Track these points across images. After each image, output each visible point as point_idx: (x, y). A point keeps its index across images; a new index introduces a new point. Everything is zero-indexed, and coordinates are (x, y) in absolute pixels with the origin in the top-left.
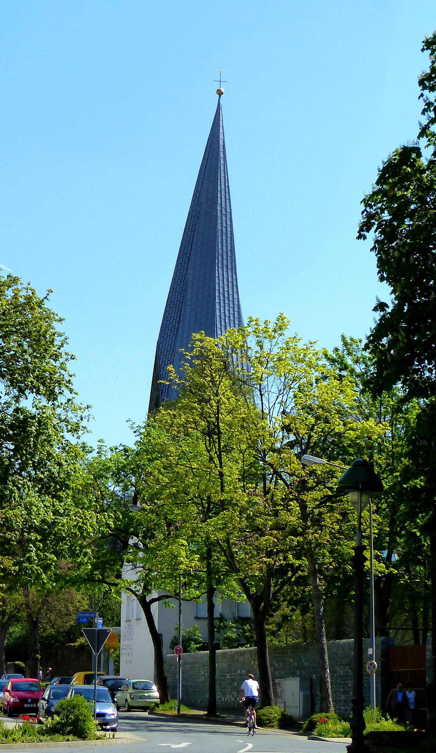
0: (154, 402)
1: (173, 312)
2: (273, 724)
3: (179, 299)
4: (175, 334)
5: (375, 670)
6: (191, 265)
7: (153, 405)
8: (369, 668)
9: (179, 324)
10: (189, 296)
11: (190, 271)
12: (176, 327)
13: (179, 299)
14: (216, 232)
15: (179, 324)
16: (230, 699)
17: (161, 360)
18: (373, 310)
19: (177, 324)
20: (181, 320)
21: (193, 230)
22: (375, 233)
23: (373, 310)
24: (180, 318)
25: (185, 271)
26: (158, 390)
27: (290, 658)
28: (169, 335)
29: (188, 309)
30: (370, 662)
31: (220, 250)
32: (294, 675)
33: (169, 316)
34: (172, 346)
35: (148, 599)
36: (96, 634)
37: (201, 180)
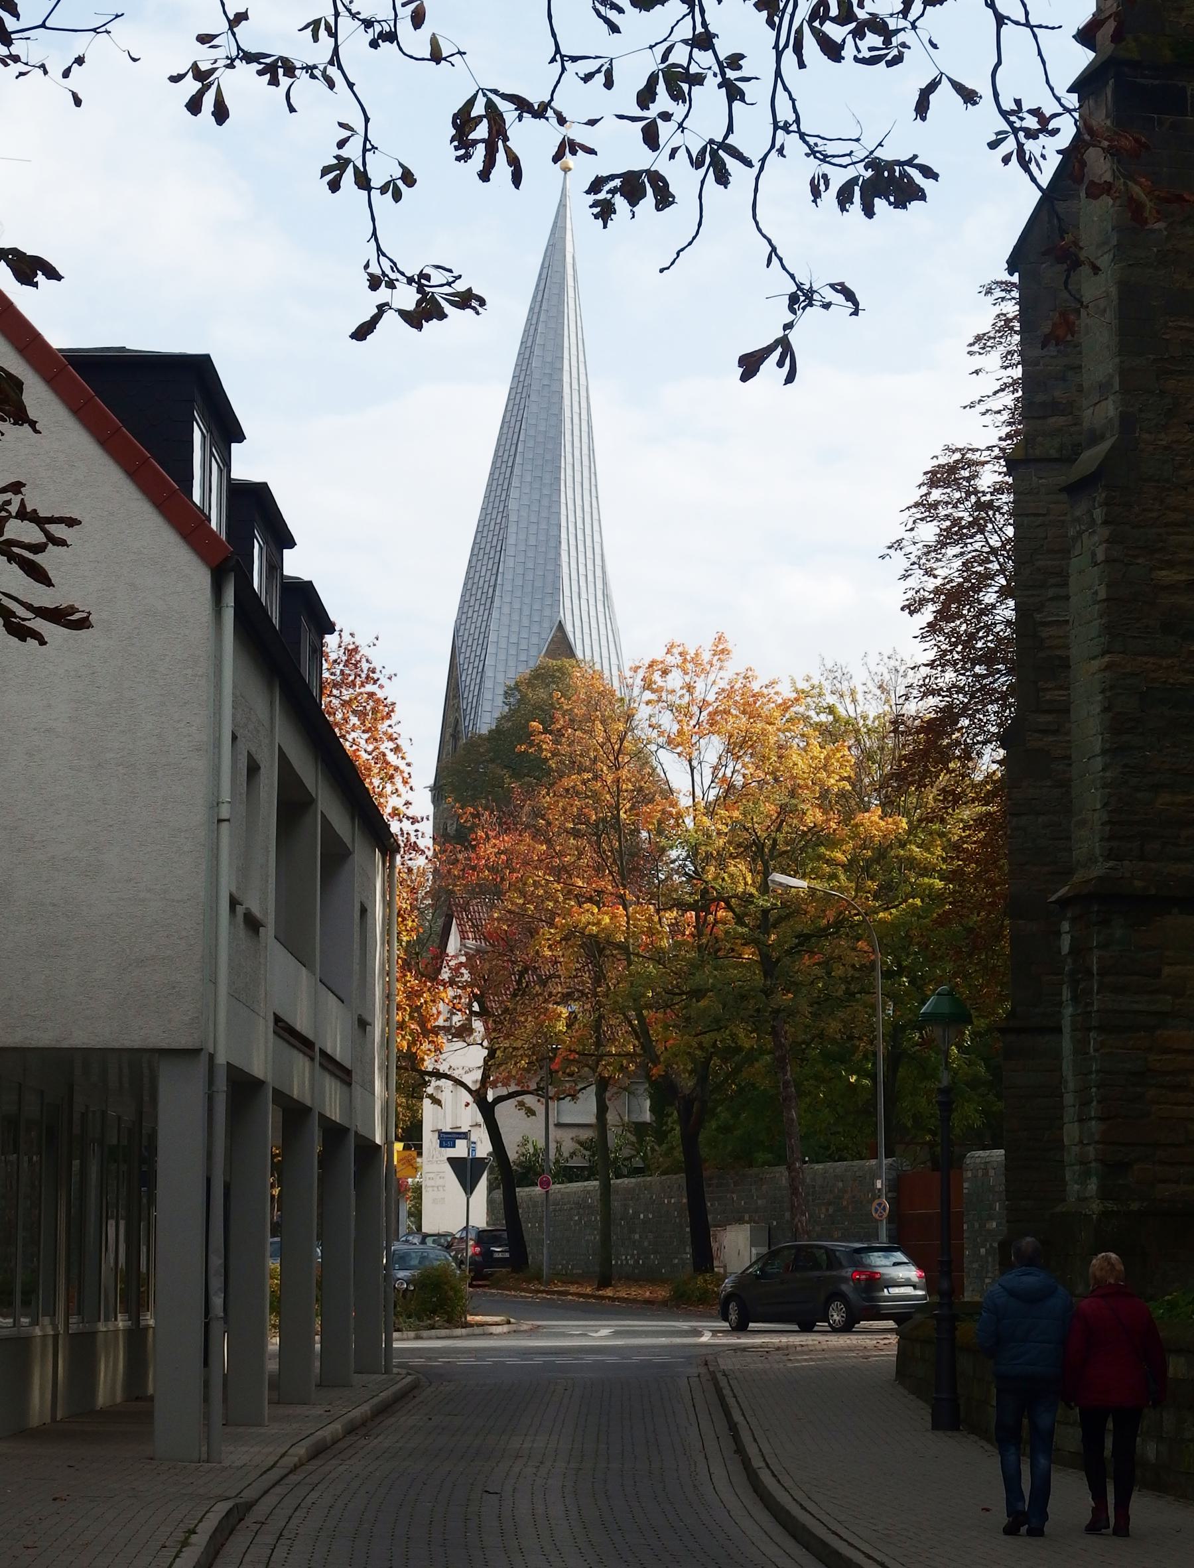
0: (450, 730)
1: (484, 568)
2: (18, 1302)
3: (494, 543)
4: (488, 607)
5: (886, 1214)
6: (515, 482)
7: (447, 736)
8: (876, 1210)
9: (494, 591)
10: (511, 540)
11: (514, 493)
12: (490, 595)
13: (494, 543)
14: (560, 421)
15: (494, 591)
16: (627, 1263)
17: (462, 655)
18: (726, 188)
19: (491, 590)
20: (498, 582)
21: (519, 418)
22: (832, 286)
23: (726, 188)
24: (496, 580)
25: (504, 493)
26: (458, 708)
27: (733, 1193)
28: (476, 609)
29: (510, 562)
30: (877, 1201)
31: (569, 456)
32: (740, 1221)
33: (477, 575)
34: (483, 630)
35: (490, 1098)
36: (469, 1165)
37: (533, 327)
